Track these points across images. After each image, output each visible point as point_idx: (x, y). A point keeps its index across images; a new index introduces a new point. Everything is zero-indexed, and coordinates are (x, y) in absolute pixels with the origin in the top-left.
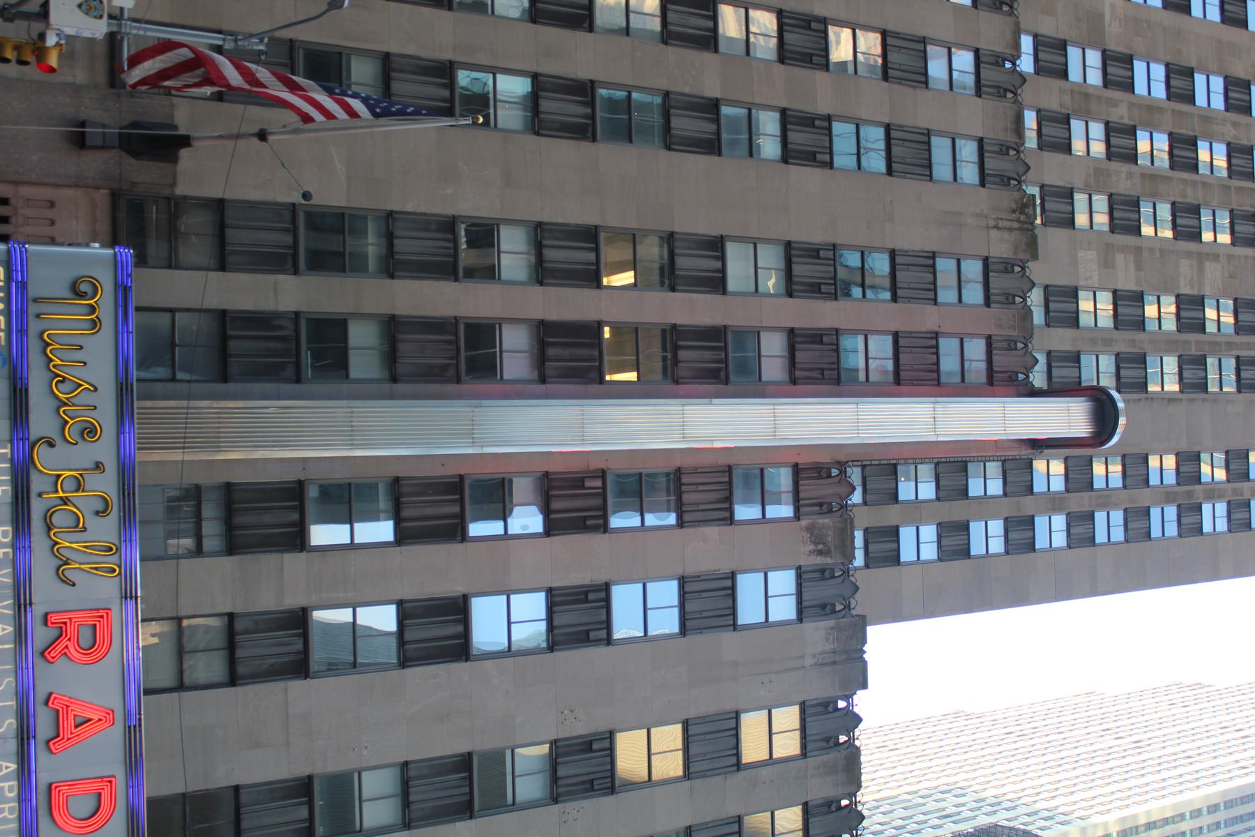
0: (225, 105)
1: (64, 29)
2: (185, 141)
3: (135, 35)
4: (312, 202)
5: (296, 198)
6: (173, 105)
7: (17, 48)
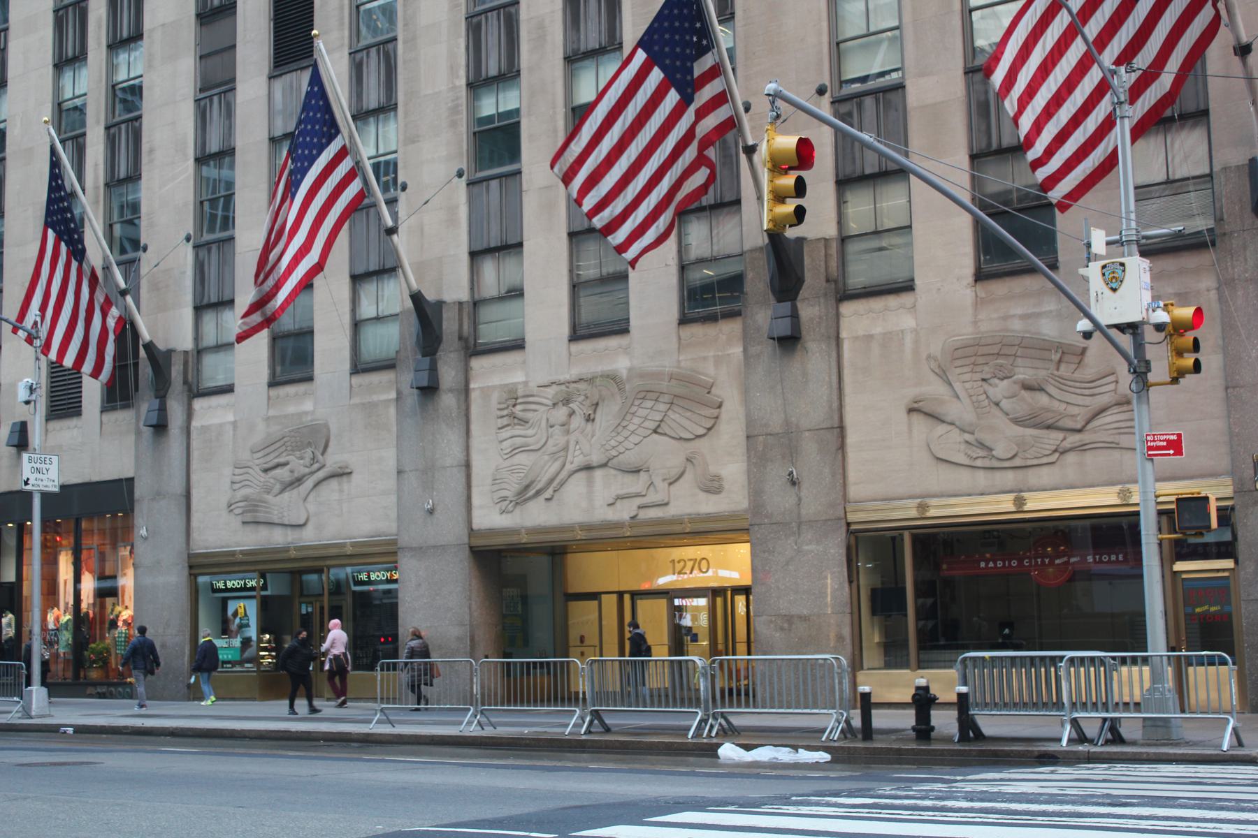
0: (1212, 106)
1: (1145, 304)
2: (417, 298)
3: (1138, 223)
4: (465, 168)
5: (463, 182)
6: (1225, 169)
7: (1179, 353)
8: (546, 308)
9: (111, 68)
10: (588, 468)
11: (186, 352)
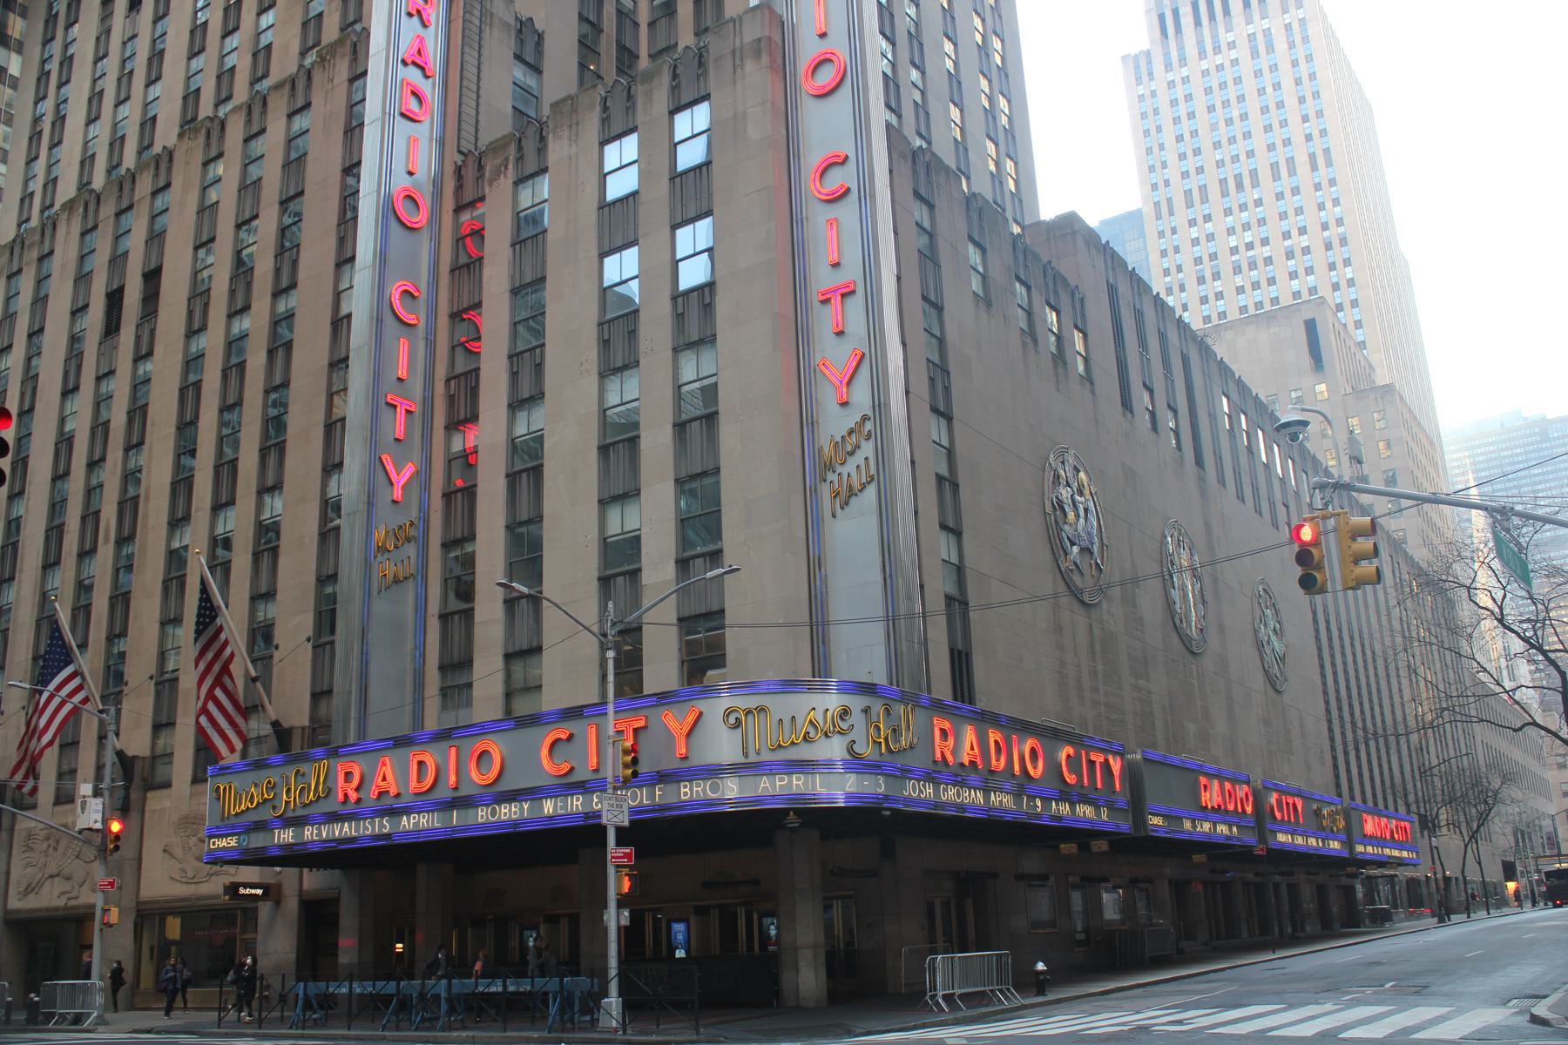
5: (310, 646)
8: (182, 765)
9: (260, 507)
10: (52, 876)
11: (303, 728)
